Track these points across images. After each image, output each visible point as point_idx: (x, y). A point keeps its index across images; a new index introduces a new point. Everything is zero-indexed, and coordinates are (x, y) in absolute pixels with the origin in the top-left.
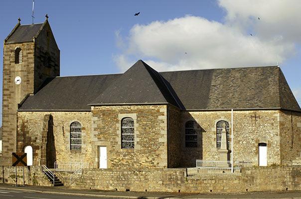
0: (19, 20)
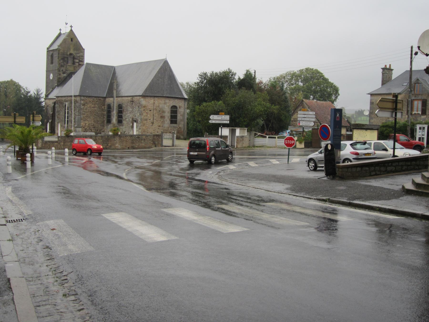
0: (71, 27)
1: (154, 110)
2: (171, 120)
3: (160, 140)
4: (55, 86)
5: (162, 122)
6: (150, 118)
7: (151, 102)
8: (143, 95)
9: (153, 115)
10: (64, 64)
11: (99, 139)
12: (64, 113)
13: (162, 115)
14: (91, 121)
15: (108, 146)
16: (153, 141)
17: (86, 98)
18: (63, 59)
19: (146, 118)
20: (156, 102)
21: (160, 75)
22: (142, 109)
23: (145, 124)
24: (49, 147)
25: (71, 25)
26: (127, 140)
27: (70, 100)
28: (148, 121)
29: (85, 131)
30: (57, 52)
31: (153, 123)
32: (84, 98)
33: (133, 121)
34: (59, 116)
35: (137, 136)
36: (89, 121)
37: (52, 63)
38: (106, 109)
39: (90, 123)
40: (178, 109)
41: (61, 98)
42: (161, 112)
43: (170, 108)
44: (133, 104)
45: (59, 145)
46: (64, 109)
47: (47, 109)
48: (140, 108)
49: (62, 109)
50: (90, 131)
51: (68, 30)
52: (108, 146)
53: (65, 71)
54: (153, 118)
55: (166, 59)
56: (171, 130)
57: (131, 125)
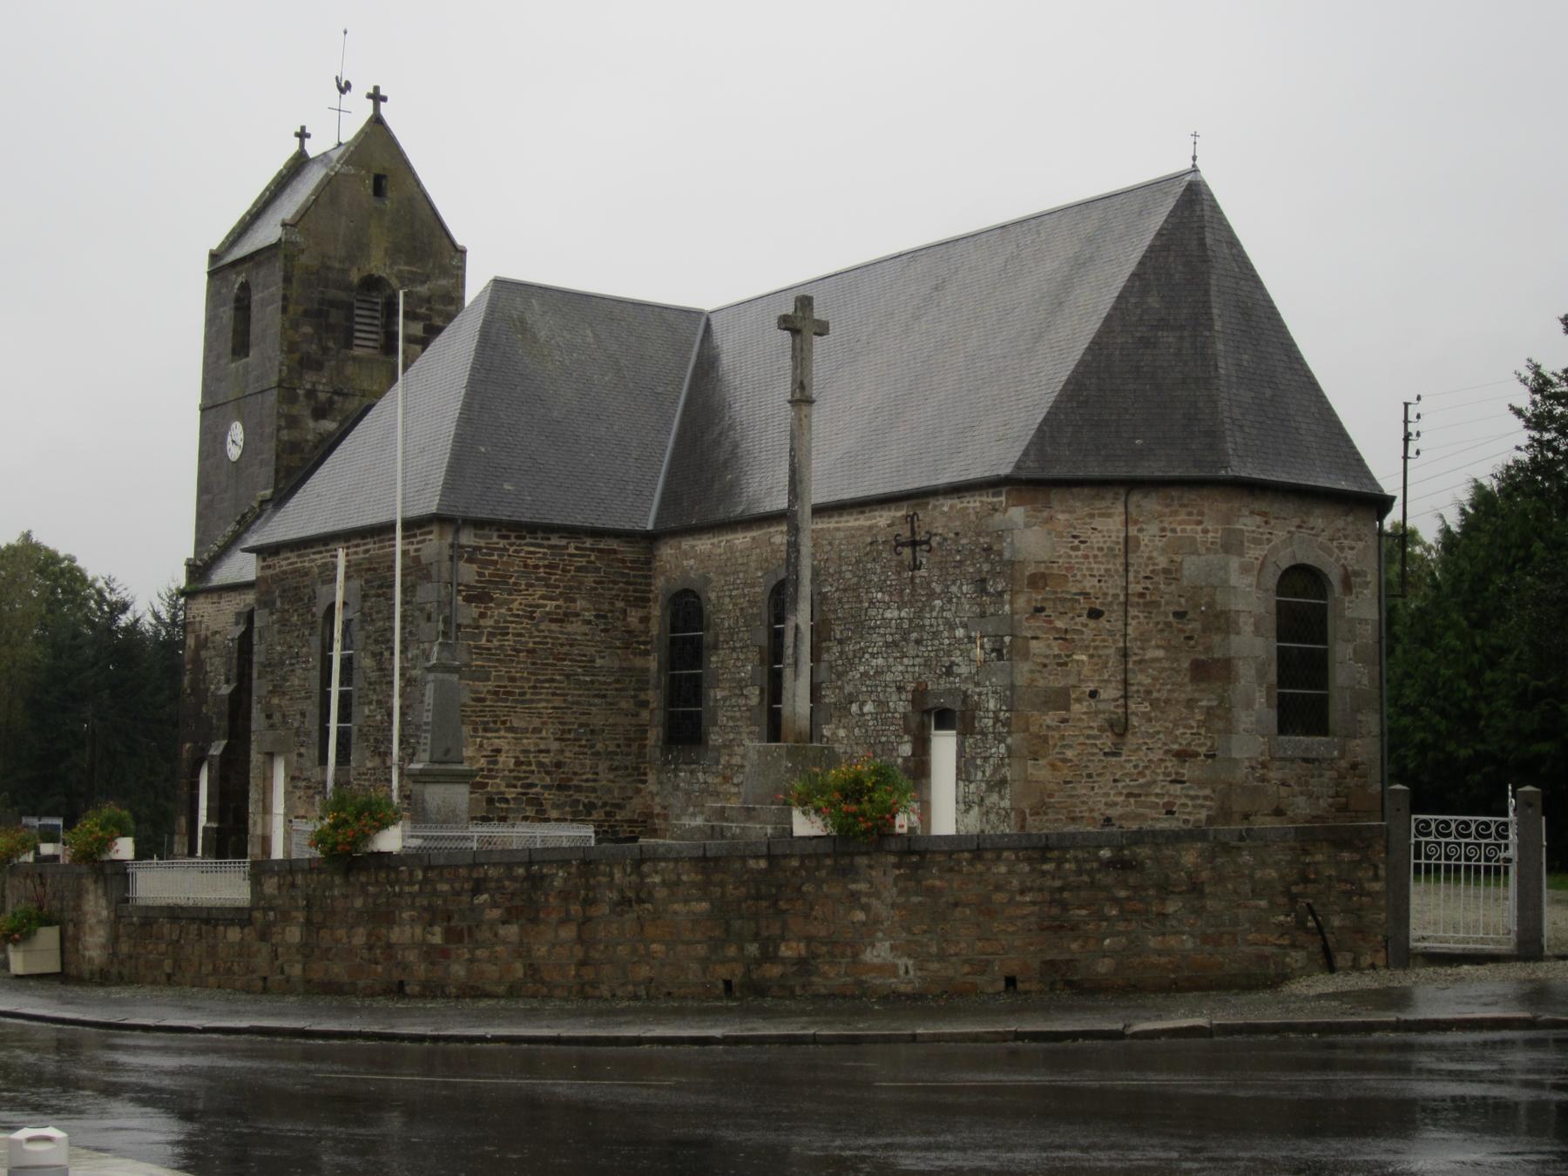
0: (377, 97)
1: (1126, 603)
2: (1281, 697)
3: (1377, 886)
4: (255, 504)
5: (1209, 712)
6: (1092, 686)
7: (1096, 540)
8: (1024, 475)
9: (1125, 654)
10: (325, 350)
11: (672, 885)
12: (316, 674)
13: (1208, 649)
14: (537, 730)
15: (774, 958)
16: (1293, 898)
17: (502, 543)
18: (318, 314)
19: (1057, 682)
20: (1149, 536)
21: (1153, 301)
22: (1021, 602)
23: (1045, 739)
24: (168, 966)
25: (376, 89)
26: (999, 897)
27: (370, 560)
28: (1076, 707)
29: (485, 819)
30: (279, 264)
31: (1120, 728)
32: (482, 543)
33: (928, 712)
34: (275, 701)
35: (1105, 853)
36: (526, 730)
37: (241, 347)
38: (655, 631)
39: (526, 752)
40: (1330, 602)
41: (293, 557)
42: (1194, 626)
43: (1272, 582)
44: (916, 567)
45: (265, 949)
46: (315, 642)
47: (198, 662)
48: (1000, 594)
49: (306, 643)
50: (530, 812)
51: (353, 124)
52: (774, 958)
53: (331, 402)
54: (1126, 682)
55: (1195, 170)
56: (1284, 791)
57: (906, 749)
